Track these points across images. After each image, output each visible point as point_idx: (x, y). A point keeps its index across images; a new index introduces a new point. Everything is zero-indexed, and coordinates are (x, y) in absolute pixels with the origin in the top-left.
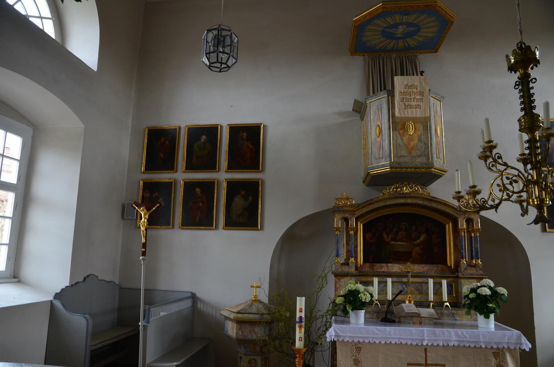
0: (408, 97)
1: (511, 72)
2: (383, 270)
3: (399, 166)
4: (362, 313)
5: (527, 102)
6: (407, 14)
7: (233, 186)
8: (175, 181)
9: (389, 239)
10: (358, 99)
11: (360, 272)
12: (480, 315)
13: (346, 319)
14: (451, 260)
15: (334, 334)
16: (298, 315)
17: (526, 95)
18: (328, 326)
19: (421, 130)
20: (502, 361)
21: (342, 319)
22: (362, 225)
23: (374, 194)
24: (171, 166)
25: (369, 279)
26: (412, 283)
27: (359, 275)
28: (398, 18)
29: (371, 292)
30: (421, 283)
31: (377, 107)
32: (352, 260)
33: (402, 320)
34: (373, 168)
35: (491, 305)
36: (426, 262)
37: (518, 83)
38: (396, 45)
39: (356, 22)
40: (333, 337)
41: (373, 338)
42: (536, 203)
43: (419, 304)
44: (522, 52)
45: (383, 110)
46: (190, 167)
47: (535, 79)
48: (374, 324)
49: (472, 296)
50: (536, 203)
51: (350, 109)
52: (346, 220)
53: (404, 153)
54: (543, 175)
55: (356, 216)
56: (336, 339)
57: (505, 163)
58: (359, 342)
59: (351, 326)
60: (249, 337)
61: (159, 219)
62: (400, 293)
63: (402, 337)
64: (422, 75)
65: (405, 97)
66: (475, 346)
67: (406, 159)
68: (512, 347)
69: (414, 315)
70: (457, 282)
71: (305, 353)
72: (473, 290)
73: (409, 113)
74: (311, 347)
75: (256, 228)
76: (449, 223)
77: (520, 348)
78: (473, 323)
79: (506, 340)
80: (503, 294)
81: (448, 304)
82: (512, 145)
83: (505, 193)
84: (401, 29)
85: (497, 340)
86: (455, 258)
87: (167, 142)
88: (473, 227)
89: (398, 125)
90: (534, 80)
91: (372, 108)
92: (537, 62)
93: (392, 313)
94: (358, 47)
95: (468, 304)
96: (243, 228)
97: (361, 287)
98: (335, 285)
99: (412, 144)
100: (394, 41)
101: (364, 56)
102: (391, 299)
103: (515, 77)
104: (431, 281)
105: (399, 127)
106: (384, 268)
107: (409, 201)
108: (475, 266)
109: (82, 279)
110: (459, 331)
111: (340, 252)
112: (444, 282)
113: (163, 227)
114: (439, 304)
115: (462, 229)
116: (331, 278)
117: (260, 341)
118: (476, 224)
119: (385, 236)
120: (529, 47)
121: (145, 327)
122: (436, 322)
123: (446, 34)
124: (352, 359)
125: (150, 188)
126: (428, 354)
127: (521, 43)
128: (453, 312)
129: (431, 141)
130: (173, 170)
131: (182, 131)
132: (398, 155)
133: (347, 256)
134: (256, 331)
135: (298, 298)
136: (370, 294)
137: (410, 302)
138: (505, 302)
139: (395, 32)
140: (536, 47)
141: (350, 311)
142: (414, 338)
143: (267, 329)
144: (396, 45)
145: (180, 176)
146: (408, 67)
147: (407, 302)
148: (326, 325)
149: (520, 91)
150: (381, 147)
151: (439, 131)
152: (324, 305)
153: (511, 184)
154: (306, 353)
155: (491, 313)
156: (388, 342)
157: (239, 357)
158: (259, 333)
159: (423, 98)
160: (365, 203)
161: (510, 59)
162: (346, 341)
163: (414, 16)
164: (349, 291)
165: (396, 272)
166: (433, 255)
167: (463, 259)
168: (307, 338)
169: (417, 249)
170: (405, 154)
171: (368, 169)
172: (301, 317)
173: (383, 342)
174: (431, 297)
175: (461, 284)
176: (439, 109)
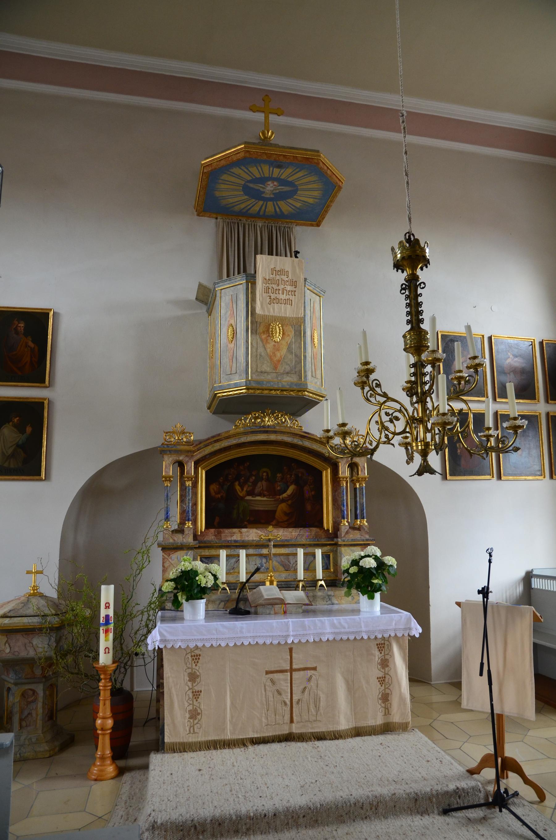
1: (397, 271)
2: (234, 538)
3: (259, 387)
4: (201, 604)
5: (414, 313)
6: (279, 167)
9: (244, 493)
10: (205, 283)
11: (200, 542)
12: (363, 595)
13: (179, 614)
14: (328, 522)
15: (158, 638)
17: (413, 304)
18: (150, 626)
19: (291, 336)
20: (388, 654)
21: (173, 614)
22: (204, 472)
23: (224, 426)
25: (213, 552)
26: (275, 555)
27: (200, 547)
28: (266, 170)
29: (214, 573)
30: (288, 555)
31: (231, 296)
32: (189, 524)
33: (260, 610)
34: (222, 388)
35: (375, 581)
36: (296, 525)
37: (404, 286)
38: (263, 208)
39: (209, 165)
40: (157, 644)
41: (217, 639)
42: (420, 448)
43: (285, 586)
44: (410, 245)
45: (239, 302)
47: (424, 284)
48: (220, 618)
49: (353, 570)
50: (420, 448)
51: (193, 297)
52: (181, 465)
53: (266, 367)
54: (428, 412)
55: (196, 458)
56: (161, 647)
57: (384, 393)
58: (197, 647)
59: (186, 623)
60: (23, 654)
62: (257, 570)
63: (258, 635)
64: (296, 257)
65: (270, 286)
66: (355, 638)
67: (269, 377)
68: (400, 635)
69: (276, 601)
70: (336, 551)
71: (115, 671)
72: (355, 563)
73: (271, 310)
74: (125, 661)
75: (37, 477)
76: (326, 470)
77: (409, 635)
78: (355, 606)
79: (393, 626)
80: (391, 566)
81: (323, 583)
82: (395, 370)
83: (383, 435)
84: (270, 188)
85: (382, 628)
86: (334, 518)
88: (358, 474)
89: (259, 326)
90: (422, 285)
91: (223, 299)
92: (426, 262)
93: (246, 600)
94: (208, 205)
95: (348, 581)
96: (16, 477)
97: (199, 566)
98: (163, 563)
99: (278, 354)
100: (261, 203)
101: (217, 218)
102: (245, 581)
103: (401, 277)
104: (301, 552)
105: (261, 329)
107: (273, 437)
108: (359, 529)
110: (335, 619)
111: (171, 514)
112: (319, 553)
114: (312, 584)
115: (343, 478)
116: (157, 554)
117: (40, 659)
118: (362, 471)
119: (238, 488)
120: (417, 241)
122: (307, 610)
123: (331, 201)
124: (186, 674)
126: (294, 655)
127: (410, 233)
128: (330, 593)
129: (305, 352)
132: (259, 370)
133: (181, 519)
134: (34, 643)
135: (103, 587)
136: (213, 575)
137: (271, 583)
138: (394, 575)
139: (261, 189)
140: (426, 242)
141: (184, 601)
142: (275, 634)
143: (53, 639)
144: (263, 208)
146: (278, 243)
147: (268, 583)
148: (147, 626)
149: (407, 297)
150: (234, 357)
151: (316, 339)
152: (145, 595)
153: (391, 421)
154: (117, 672)
155: (376, 592)
156: (239, 644)
157: (5, 690)
159: (296, 289)
160: (208, 439)
161: (396, 253)
162: (178, 647)
163: (289, 171)
164: (182, 572)
165: (253, 540)
166: (304, 513)
167: (344, 518)
168: (118, 648)
169: (283, 506)
170: (268, 369)
171: (213, 389)
172: (107, 617)
173: (231, 645)
174: (301, 574)
175: (341, 554)
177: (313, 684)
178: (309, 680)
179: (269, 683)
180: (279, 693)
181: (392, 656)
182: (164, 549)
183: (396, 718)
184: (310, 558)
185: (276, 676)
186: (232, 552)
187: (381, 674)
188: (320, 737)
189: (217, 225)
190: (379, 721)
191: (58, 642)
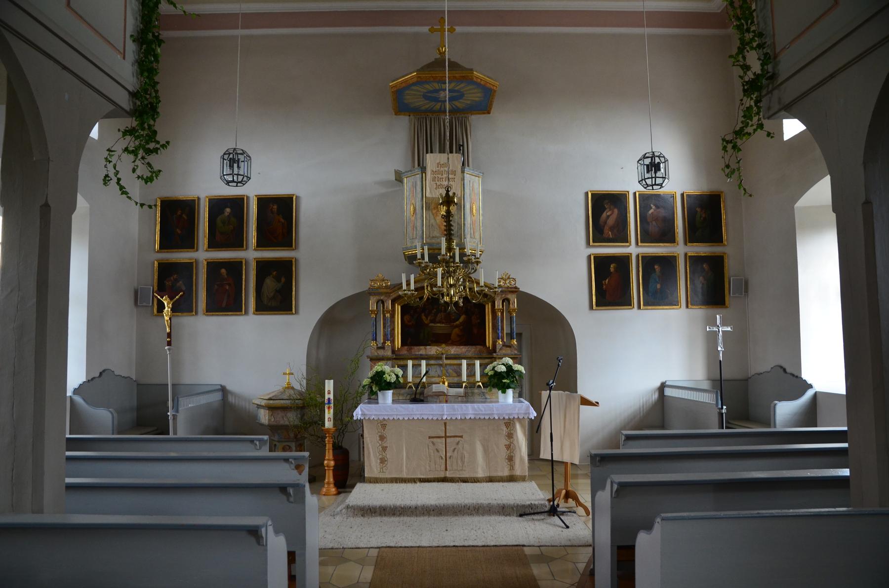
0: (440, 176)
2: (421, 352)
4: (390, 393)
7: (264, 267)
8: (197, 261)
14: (489, 342)
16: (327, 397)
24: (189, 243)
33: (429, 399)
36: (461, 344)
39: (392, 87)
46: (213, 244)
48: (404, 402)
60: (282, 422)
61: (183, 306)
68: (521, 417)
87: (184, 216)
94: (401, 107)
104: (464, 362)
106: (422, 350)
109: (98, 375)
112: (478, 363)
113: (185, 314)
114: (472, 385)
119: (424, 317)
121: (175, 417)
125: (166, 271)
130: (193, 248)
131: (202, 202)
145: (202, 255)
158: (292, 418)
169: (456, 330)
172: (329, 399)
174: (464, 378)
176: (476, 186)
177: (460, 446)
178: (458, 443)
179: (431, 444)
180: (438, 451)
181: (516, 431)
182: (371, 360)
183: (518, 472)
184: (471, 367)
185: (435, 440)
186: (416, 362)
187: (508, 443)
188: (465, 480)
189: (410, 121)
190: (506, 473)
191: (303, 416)
